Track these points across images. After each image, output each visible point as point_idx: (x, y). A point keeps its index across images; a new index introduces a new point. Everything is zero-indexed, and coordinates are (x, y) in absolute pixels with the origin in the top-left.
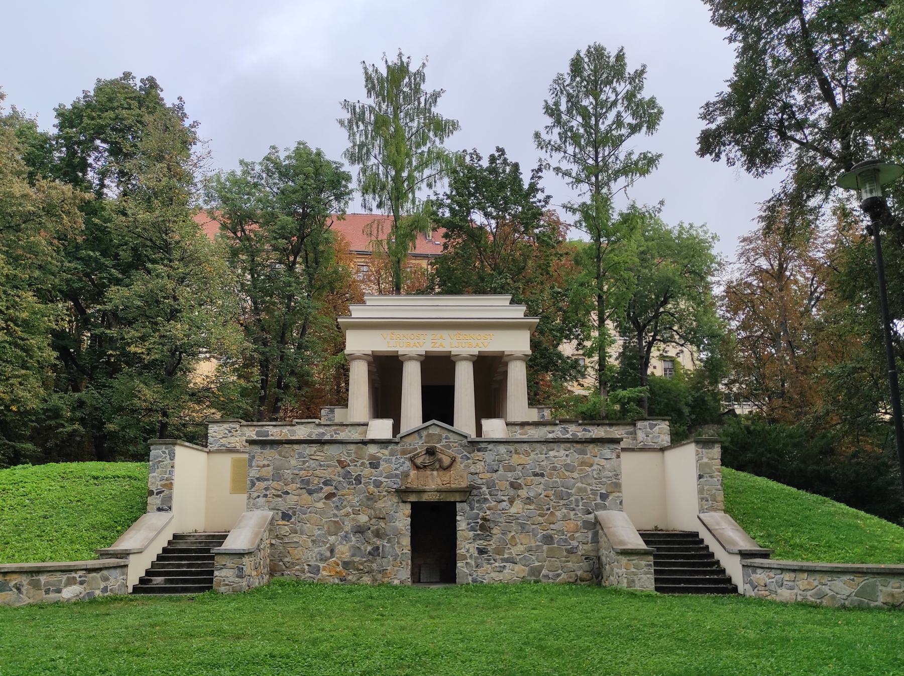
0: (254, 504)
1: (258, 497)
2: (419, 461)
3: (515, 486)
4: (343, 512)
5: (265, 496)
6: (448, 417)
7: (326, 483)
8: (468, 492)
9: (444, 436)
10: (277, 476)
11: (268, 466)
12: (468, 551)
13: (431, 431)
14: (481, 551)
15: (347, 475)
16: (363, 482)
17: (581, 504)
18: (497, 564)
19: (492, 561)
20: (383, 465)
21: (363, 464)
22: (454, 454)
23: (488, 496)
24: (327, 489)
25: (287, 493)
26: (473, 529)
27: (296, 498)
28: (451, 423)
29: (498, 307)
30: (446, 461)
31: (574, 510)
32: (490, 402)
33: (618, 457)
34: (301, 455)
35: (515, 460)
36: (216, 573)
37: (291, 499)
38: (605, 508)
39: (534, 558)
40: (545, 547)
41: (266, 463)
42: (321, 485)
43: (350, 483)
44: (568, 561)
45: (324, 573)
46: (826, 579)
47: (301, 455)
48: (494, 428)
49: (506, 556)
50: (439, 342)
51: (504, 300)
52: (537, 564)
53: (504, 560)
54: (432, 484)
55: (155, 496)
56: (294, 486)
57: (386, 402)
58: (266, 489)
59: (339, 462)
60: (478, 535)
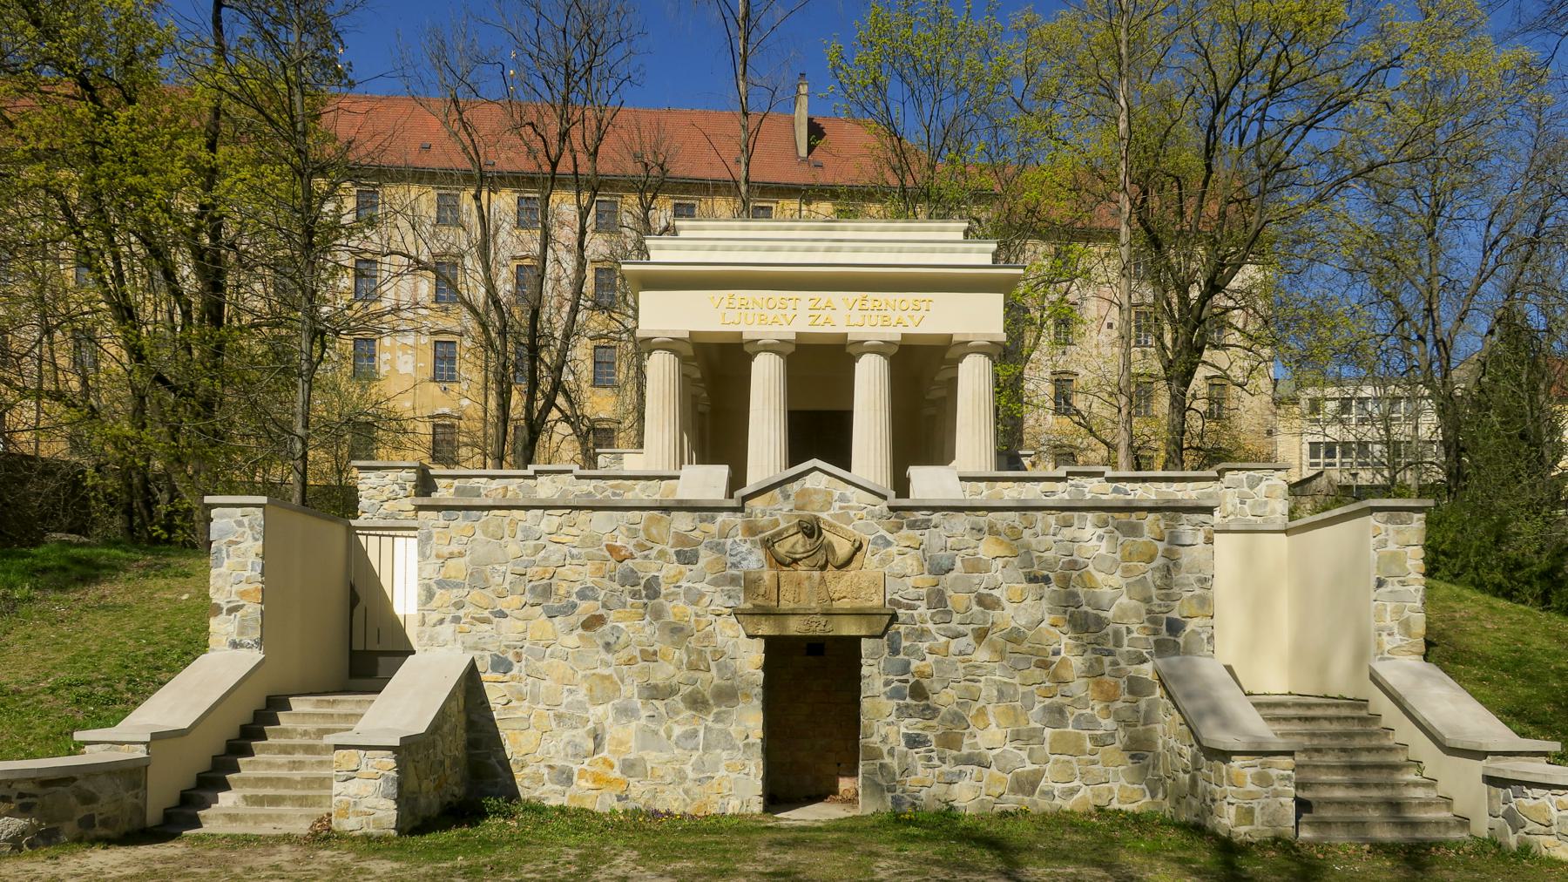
0: (431, 638)
1: (441, 621)
2: (782, 549)
5: (456, 620)
6: (840, 453)
7: (582, 595)
9: (837, 494)
10: (478, 579)
11: (461, 555)
12: (884, 740)
13: (812, 481)
16: (663, 591)
17: (1126, 642)
18: (945, 768)
19: (936, 762)
21: (662, 554)
22: (858, 535)
23: (930, 625)
24: (586, 608)
25: (502, 615)
26: (896, 694)
27: (521, 625)
28: (847, 466)
29: (943, 243)
30: (843, 549)
31: (1110, 653)
32: (921, 432)
33: (1209, 541)
36: (337, 787)
37: (510, 629)
39: (1024, 754)
40: (1048, 731)
41: (455, 548)
42: (574, 598)
43: (634, 595)
44: (1094, 763)
45: (583, 783)
48: (927, 482)
49: (965, 751)
50: (825, 314)
51: (954, 229)
52: (1029, 767)
53: (958, 761)
54: (809, 600)
55: (223, 616)
57: (715, 427)
58: (459, 605)
59: (612, 549)
60: (907, 706)
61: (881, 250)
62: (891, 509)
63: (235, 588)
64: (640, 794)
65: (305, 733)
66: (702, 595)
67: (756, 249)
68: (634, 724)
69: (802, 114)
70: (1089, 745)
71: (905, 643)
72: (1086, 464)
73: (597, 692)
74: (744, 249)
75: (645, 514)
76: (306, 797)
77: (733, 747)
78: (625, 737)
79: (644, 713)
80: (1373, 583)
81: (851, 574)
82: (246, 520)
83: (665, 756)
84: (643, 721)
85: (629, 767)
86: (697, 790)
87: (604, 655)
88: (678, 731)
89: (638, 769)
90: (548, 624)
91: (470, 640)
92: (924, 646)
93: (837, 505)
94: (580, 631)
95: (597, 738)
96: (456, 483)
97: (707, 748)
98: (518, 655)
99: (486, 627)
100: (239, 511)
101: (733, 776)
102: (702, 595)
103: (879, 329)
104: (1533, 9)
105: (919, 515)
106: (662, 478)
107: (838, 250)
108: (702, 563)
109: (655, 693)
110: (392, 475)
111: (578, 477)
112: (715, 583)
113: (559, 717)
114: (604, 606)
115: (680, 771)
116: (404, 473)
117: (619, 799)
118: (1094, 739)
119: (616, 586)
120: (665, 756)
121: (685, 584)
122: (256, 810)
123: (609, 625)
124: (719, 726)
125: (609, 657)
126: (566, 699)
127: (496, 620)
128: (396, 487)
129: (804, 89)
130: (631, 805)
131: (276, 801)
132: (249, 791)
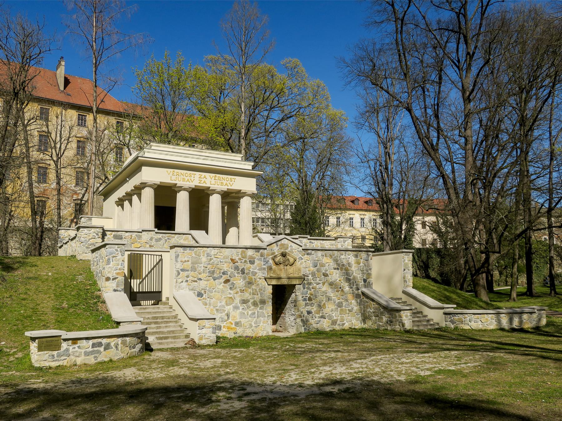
0: (179, 287)
1: (182, 282)
2: (277, 260)
5: (187, 281)
7: (224, 273)
10: (194, 269)
11: (188, 261)
15: (237, 268)
23: (312, 281)
25: (200, 279)
30: (292, 260)
34: (208, 255)
43: (238, 273)
45: (224, 329)
47: (208, 255)
50: (203, 180)
51: (238, 157)
52: (335, 318)
54: (284, 275)
55: (111, 281)
58: (188, 277)
59: (232, 260)
61: (220, 161)
62: (303, 250)
63: (115, 272)
64: (240, 331)
65: (148, 318)
66: (256, 273)
67: (181, 156)
68: (238, 311)
69: (61, 72)
70: (348, 312)
71: (306, 286)
72: (327, 236)
73: (228, 302)
74: (177, 156)
75: (241, 250)
76: (175, 336)
77: (265, 316)
78: (236, 315)
79: (241, 308)
80: (403, 269)
81: (294, 267)
82: (119, 249)
83: (247, 320)
84: (241, 310)
85: (237, 324)
86: (255, 329)
87: (229, 291)
88: (250, 312)
89: (240, 324)
90: (214, 282)
91: (191, 287)
92: (311, 287)
93: (290, 248)
94: (223, 284)
95: (228, 315)
96: (113, 233)
97: (258, 317)
98: (205, 292)
99: (196, 283)
100: (117, 246)
101: (265, 325)
102: (256, 273)
103: (220, 186)
105: (309, 251)
106: (184, 234)
107: (207, 160)
108: (256, 264)
109: (244, 302)
110: (93, 230)
111: (156, 233)
112: (259, 270)
113: (217, 310)
114: (230, 276)
115: (251, 324)
116: (98, 229)
117: (234, 333)
118: (349, 310)
119: (233, 270)
120: (247, 320)
121: (252, 270)
122: (160, 341)
123: (231, 282)
124: (261, 311)
125: (231, 292)
126: (219, 304)
127: (198, 281)
128: (95, 234)
129: (63, 63)
130: (238, 335)
131: (166, 338)
132: (158, 336)
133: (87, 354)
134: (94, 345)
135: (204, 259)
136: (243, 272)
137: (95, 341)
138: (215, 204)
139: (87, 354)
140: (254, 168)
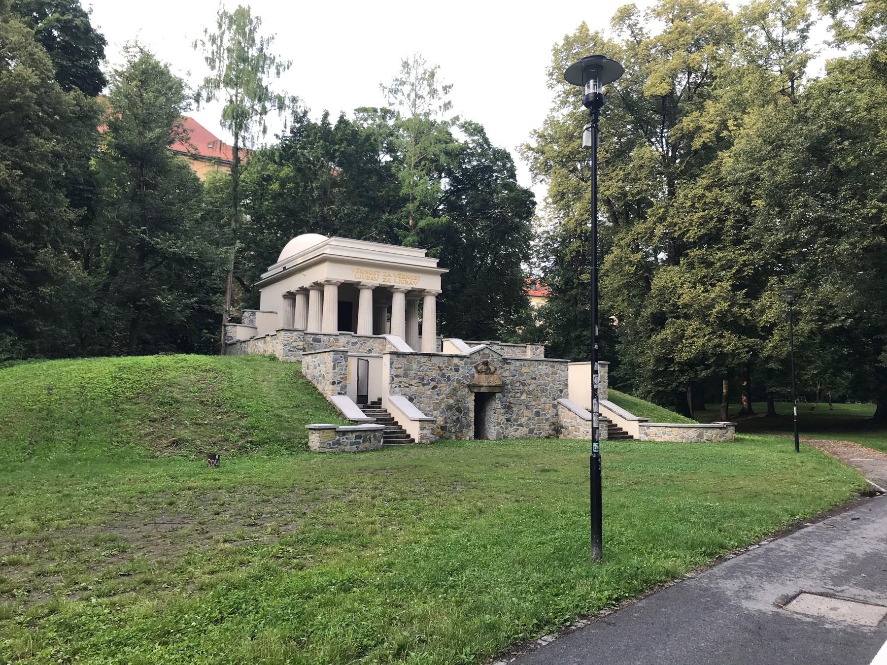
2: (479, 368)
3: (523, 384)
4: (441, 397)
7: (432, 380)
8: (502, 388)
10: (406, 375)
14: (508, 420)
15: (443, 375)
20: (461, 370)
24: (433, 384)
28: (356, 333)
30: (492, 369)
34: (419, 362)
35: (524, 370)
38: (561, 397)
46: (686, 430)
47: (419, 362)
51: (422, 253)
54: (484, 381)
56: (415, 381)
58: (400, 382)
104: (883, 58)
110: (295, 333)
126: (427, 409)
133: (352, 444)
134: (356, 438)
135: (415, 366)
136: (449, 378)
137: (357, 434)
138: (399, 303)
139: (352, 444)
140: (439, 265)
